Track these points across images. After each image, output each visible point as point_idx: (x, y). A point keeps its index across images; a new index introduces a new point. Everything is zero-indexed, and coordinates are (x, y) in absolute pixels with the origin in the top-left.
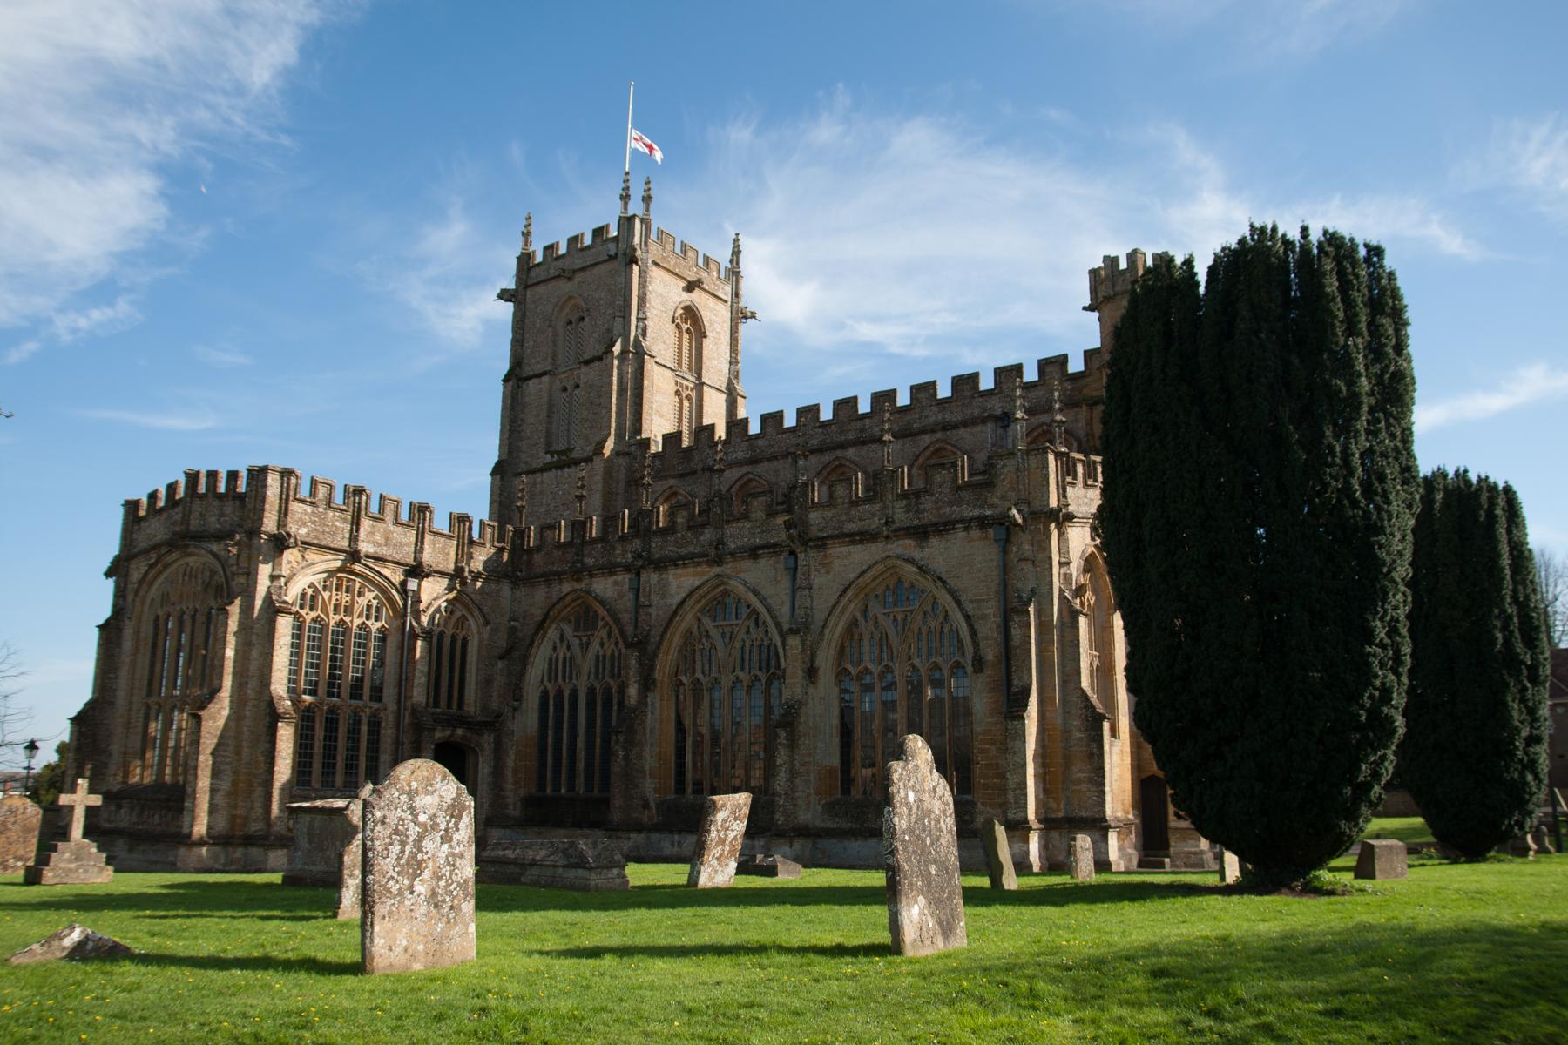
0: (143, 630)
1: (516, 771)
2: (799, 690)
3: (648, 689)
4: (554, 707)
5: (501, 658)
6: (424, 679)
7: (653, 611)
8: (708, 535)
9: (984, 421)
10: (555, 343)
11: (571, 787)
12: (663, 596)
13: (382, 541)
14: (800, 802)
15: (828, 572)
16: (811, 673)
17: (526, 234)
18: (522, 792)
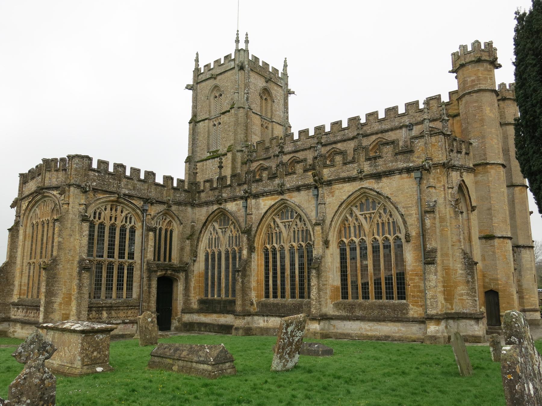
0: (28, 230)
1: (195, 288)
2: (321, 251)
3: (252, 251)
4: (212, 259)
5: (188, 239)
6: (152, 249)
7: (253, 216)
8: (277, 181)
9: (401, 128)
10: (210, 106)
11: (219, 295)
12: (258, 209)
13: (132, 188)
14: (323, 303)
15: (333, 196)
16: (326, 243)
17: (197, 60)
18: (198, 297)
